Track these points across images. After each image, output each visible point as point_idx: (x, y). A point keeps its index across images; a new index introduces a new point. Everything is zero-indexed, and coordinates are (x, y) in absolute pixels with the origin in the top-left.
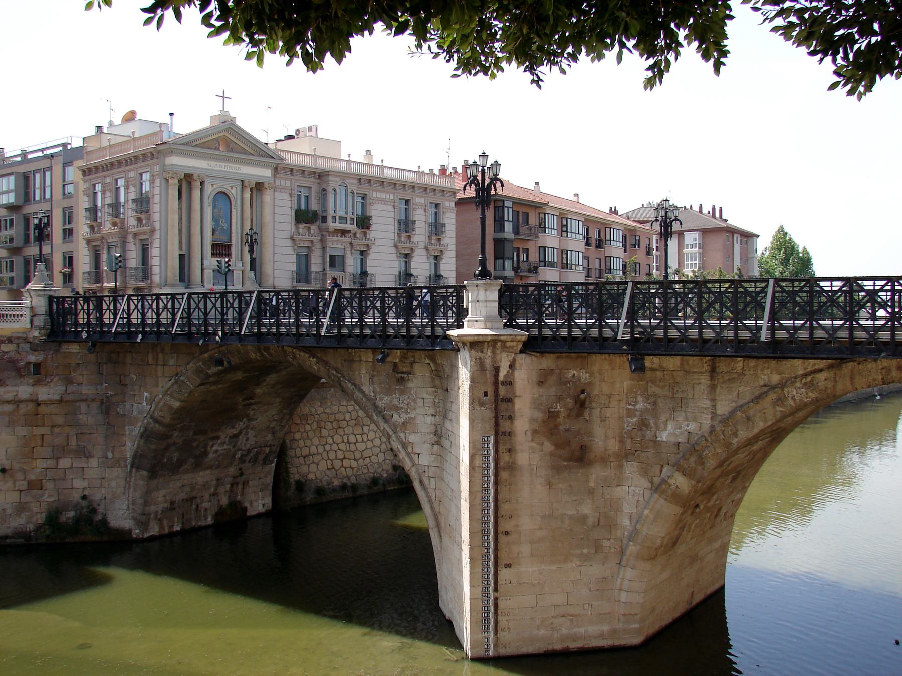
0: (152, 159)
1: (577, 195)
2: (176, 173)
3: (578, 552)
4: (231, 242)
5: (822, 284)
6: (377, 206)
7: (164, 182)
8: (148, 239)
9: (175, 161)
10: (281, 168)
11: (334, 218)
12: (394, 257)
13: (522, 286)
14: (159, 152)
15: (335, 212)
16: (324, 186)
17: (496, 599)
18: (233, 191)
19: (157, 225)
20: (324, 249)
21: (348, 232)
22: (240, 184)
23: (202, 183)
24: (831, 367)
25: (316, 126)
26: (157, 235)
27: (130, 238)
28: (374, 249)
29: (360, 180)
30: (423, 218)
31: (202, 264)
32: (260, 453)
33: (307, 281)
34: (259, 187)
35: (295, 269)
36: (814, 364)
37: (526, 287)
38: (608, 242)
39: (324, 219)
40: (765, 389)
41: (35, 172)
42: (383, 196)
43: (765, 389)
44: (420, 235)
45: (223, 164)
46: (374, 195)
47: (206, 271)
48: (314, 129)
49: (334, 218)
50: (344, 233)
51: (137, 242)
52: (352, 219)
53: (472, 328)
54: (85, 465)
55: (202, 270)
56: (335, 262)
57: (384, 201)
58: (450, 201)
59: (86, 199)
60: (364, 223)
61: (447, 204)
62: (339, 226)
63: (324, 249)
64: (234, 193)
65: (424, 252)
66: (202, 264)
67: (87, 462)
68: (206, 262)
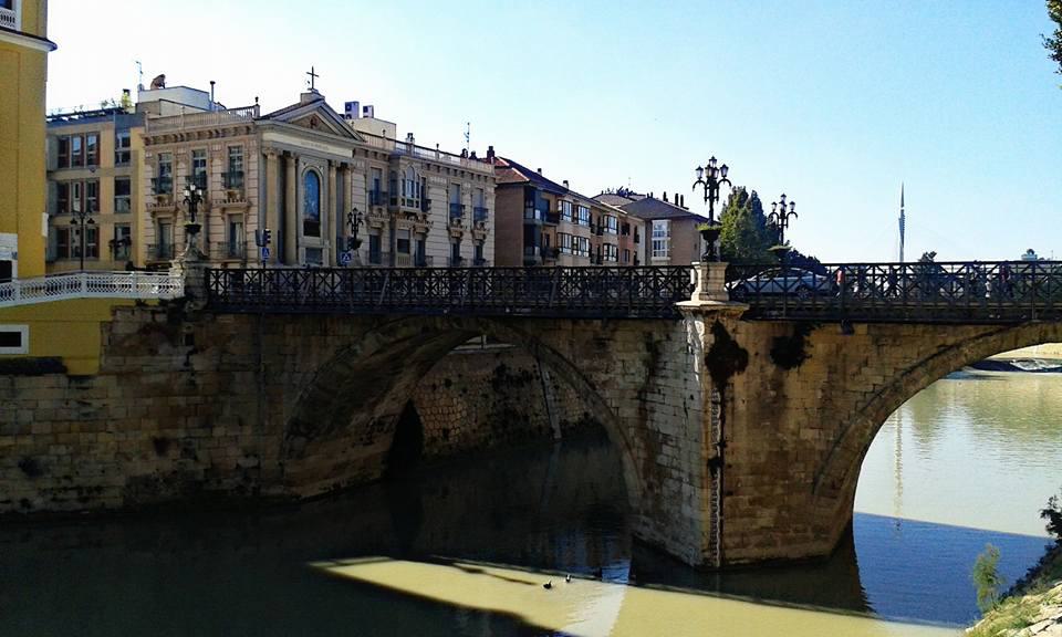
0: (248, 133)
1: (566, 182)
2: (276, 149)
3: (782, 482)
4: (319, 220)
5: (944, 266)
6: (432, 191)
7: (262, 159)
8: (170, 218)
9: (269, 136)
10: (362, 151)
11: (403, 200)
12: (446, 240)
13: (545, 268)
14: (257, 127)
15: (404, 195)
16: (393, 169)
17: (721, 521)
18: (321, 170)
19: (255, 201)
20: (392, 230)
21: (414, 214)
22: (326, 163)
23: (297, 161)
24: (1000, 331)
25: (372, 107)
26: (254, 210)
27: (216, 212)
28: (431, 232)
29: (330, 162)
30: (470, 203)
31: (297, 241)
32: (295, 428)
33: (378, 262)
34: (343, 168)
35: (368, 249)
36: (985, 329)
37: (548, 269)
38: (606, 230)
39: (394, 202)
40: (942, 348)
41: (74, 136)
42: (254, 175)
43: (942, 348)
44: (467, 221)
45: (315, 143)
46: (432, 179)
47: (300, 249)
48: (370, 110)
49: (403, 200)
50: (408, 215)
51: (226, 216)
52: (417, 202)
53: (695, 301)
54: (238, 433)
55: (297, 247)
56: (404, 245)
57: (439, 185)
58: (490, 187)
59: (149, 168)
60: (425, 204)
61: (489, 190)
62: (407, 209)
63: (392, 230)
64: (322, 171)
65: (470, 235)
66: (297, 241)
67: (241, 431)
68: (300, 239)
